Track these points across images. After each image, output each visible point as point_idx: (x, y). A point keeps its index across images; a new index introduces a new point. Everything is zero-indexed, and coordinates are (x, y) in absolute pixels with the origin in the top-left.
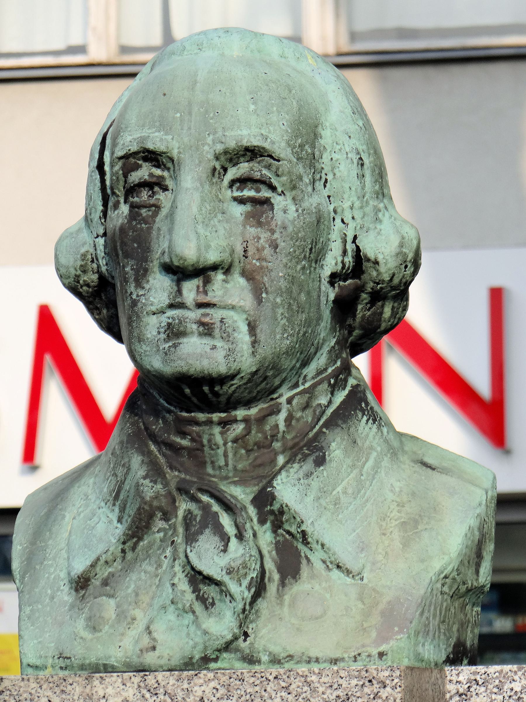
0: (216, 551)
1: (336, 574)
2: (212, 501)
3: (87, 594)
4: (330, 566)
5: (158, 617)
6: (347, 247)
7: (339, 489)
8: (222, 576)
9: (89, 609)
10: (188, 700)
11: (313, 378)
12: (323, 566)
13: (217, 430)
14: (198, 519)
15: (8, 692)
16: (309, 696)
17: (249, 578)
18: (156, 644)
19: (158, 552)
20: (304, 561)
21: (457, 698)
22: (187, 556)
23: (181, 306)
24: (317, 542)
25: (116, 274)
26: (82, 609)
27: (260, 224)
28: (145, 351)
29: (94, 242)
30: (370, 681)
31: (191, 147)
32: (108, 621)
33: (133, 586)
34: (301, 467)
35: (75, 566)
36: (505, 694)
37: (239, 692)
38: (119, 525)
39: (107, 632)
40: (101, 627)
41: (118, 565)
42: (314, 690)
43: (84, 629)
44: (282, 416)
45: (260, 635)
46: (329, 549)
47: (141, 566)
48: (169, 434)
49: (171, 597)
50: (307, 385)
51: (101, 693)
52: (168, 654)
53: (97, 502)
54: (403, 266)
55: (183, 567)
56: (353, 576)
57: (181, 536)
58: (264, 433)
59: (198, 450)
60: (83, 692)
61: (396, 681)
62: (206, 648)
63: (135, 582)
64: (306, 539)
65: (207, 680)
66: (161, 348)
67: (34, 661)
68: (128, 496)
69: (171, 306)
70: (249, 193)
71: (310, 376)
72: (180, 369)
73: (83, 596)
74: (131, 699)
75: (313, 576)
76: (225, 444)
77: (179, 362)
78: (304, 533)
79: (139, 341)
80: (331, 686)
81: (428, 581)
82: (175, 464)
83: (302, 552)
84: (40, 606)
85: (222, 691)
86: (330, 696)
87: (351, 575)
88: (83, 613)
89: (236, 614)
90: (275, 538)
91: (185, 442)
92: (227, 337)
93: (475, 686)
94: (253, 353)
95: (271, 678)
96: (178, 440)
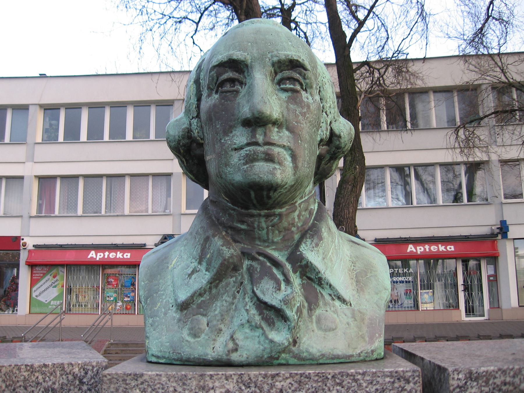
0: (274, 290)
1: (337, 303)
2: (265, 260)
7: (330, 254)
10: (271, 391)
11: (308, 195)
13: (263, 220)
14: (258, 270)
15: (147, 383)
16: (356, 389)
17: (296, 307)
21: (458, 390)
22: (253, 292)
23: (256, 144)
24: (327, 284)
27: (296, 103)
30: (398, 379)
32: (204, 331)
33: (218, 310)
34: (313, 241)
36: (490, 387)
38: (207, 273)
39: (204, 338)
40: (200, 334)
41: (206, 296)
42: (360, 385)
43: (188, 335)
45: (303, 342)
46: (334, 288)
48: (233, 222)
49: (247, 318)
50: (306, 198)
51: (211, 385)
53: (190, 260)
55: (251, 299)
57: (246, 280)
59: (252, 231)
60: (198, 384)
61: (416, 378)
62: (271, 351)
67: (157, 353)
68: (212, 256)
69: (248, 144)
70: (289, 86)
73: (186, 314)
75: (326, 304)
76: (267, 228)
78: (320, 279)
79: (226, 166)
80: (372, 383)
81: (383, 305)
84: (158, 319)
85: (296, 385)
86: (371, 389)
88: (186, 325)
90: (302, 281)
91: (243, 227)
93: (470, 382)
95: (329, 377)
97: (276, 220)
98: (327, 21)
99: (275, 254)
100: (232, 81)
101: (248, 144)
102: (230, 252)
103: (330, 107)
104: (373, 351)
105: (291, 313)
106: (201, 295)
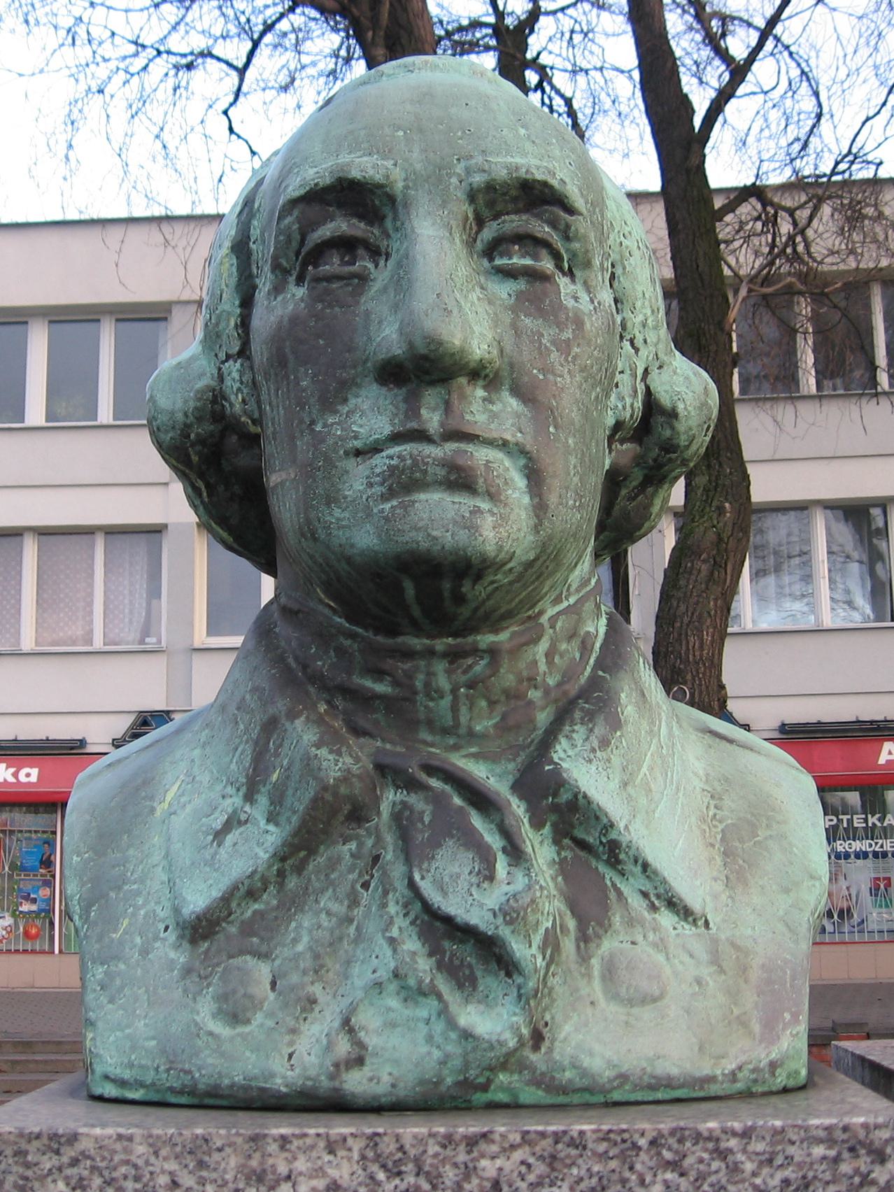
0: (474, 880)
1: (666, 919)
2: (448, 788)
3: (213, 949)
4: (656, 903)
5: (366, 1002)
7: (644, 769)
8: (497, 928)
9: (220, 979)
11: (578, 591)
12: (644, 903)
13: (440, 667)
14: (427, 819)
15: (88, 1162)
16: (724, 1181)
17: (542, 931)
18: (363, 1052)
19: (351, 877)
20: (612, 895)
22: (412, 885)
23: (421, 436)
24: (636, 861)
25: (276, 414)
26: (206, 978)
27: (541, 313)
28: (338, 519)
29: (220, 369)
30: (852, 1150)
31: (429, 177)
32: (261, 1003)
33: (305, 939)
34: (591, 730)
35: (189, 898)
37: (575, 1171)
38: (271, 828)
39: (262, 1025)
40: (249, 1014)
41: (269, 899)
42: (735, 1169)
43: (214, 1016)
45: (562, 1036)
46: (655, 873)
47: (317, 901)
48: (349, 674)
49: (392, 965)
50: (572, 600)
51: (283, 1169)
52: (390, 1074)
53: (219, 787)
55: (406, 906)
56: (695, 920)
57: (390, 848)
59: (405, 699)
60: (244, 1166)
62: (466, 1065)
63: (310, 931)
64: (616, 857)
65: (507, 1145)
66: (375, 511)
67: (118, 1071)
68: (288, 777)
69: (397, 438)
70: (519, 261)
72: (415, 546)
73: (207, 952)
74: (345, 1180)
75: (631, 922)
76: (454, 691)
77: (413, 534)
79: (328, 504)
82: (362, 722)
83: (607, 877)
84: (122, 966)
85: (540, 1168)
87: (690, 919)
88: (209, 985)
89: (523, 999)
90: (559, 854)
91: (381, 688)
94: (536, 526)
95: (643, 1142)
96: (368, 683)
97: (480, 667)
99: (479, 771)
100: (347, 245)
101: (397, 438)
102: (340, 764)
103: (644, 325)
104: (773, 1066)
105: (525, 951)
106: (252, 894)
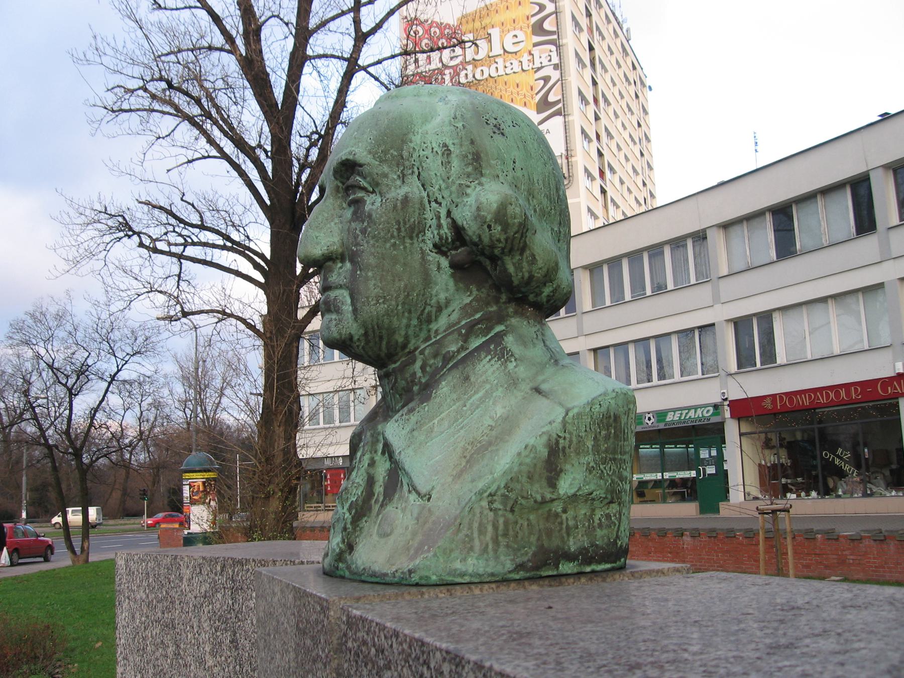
6: (442, 221)
11: (445, 331)
44: (418, 364)
54: (485, 226)
58: (406, 380)
71: (441, 330)
92: (338, 311)
98: (303, 77)
103: (440, 190)
104: (410, 572)
